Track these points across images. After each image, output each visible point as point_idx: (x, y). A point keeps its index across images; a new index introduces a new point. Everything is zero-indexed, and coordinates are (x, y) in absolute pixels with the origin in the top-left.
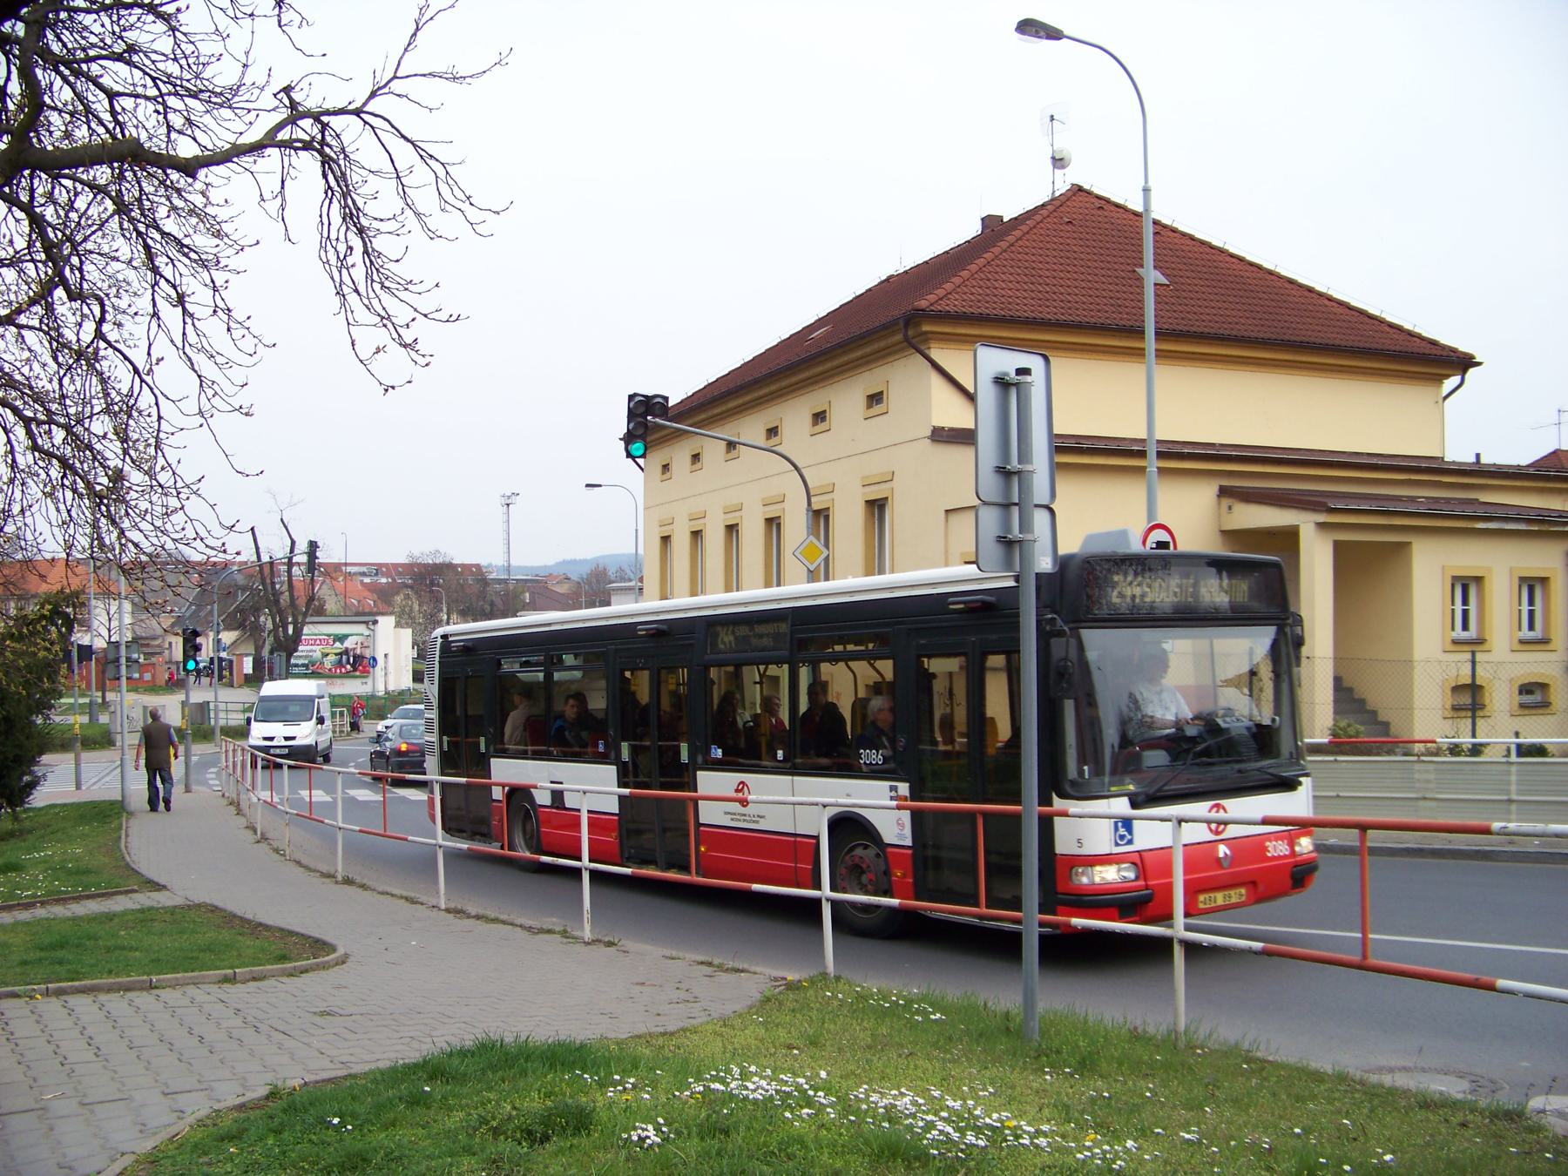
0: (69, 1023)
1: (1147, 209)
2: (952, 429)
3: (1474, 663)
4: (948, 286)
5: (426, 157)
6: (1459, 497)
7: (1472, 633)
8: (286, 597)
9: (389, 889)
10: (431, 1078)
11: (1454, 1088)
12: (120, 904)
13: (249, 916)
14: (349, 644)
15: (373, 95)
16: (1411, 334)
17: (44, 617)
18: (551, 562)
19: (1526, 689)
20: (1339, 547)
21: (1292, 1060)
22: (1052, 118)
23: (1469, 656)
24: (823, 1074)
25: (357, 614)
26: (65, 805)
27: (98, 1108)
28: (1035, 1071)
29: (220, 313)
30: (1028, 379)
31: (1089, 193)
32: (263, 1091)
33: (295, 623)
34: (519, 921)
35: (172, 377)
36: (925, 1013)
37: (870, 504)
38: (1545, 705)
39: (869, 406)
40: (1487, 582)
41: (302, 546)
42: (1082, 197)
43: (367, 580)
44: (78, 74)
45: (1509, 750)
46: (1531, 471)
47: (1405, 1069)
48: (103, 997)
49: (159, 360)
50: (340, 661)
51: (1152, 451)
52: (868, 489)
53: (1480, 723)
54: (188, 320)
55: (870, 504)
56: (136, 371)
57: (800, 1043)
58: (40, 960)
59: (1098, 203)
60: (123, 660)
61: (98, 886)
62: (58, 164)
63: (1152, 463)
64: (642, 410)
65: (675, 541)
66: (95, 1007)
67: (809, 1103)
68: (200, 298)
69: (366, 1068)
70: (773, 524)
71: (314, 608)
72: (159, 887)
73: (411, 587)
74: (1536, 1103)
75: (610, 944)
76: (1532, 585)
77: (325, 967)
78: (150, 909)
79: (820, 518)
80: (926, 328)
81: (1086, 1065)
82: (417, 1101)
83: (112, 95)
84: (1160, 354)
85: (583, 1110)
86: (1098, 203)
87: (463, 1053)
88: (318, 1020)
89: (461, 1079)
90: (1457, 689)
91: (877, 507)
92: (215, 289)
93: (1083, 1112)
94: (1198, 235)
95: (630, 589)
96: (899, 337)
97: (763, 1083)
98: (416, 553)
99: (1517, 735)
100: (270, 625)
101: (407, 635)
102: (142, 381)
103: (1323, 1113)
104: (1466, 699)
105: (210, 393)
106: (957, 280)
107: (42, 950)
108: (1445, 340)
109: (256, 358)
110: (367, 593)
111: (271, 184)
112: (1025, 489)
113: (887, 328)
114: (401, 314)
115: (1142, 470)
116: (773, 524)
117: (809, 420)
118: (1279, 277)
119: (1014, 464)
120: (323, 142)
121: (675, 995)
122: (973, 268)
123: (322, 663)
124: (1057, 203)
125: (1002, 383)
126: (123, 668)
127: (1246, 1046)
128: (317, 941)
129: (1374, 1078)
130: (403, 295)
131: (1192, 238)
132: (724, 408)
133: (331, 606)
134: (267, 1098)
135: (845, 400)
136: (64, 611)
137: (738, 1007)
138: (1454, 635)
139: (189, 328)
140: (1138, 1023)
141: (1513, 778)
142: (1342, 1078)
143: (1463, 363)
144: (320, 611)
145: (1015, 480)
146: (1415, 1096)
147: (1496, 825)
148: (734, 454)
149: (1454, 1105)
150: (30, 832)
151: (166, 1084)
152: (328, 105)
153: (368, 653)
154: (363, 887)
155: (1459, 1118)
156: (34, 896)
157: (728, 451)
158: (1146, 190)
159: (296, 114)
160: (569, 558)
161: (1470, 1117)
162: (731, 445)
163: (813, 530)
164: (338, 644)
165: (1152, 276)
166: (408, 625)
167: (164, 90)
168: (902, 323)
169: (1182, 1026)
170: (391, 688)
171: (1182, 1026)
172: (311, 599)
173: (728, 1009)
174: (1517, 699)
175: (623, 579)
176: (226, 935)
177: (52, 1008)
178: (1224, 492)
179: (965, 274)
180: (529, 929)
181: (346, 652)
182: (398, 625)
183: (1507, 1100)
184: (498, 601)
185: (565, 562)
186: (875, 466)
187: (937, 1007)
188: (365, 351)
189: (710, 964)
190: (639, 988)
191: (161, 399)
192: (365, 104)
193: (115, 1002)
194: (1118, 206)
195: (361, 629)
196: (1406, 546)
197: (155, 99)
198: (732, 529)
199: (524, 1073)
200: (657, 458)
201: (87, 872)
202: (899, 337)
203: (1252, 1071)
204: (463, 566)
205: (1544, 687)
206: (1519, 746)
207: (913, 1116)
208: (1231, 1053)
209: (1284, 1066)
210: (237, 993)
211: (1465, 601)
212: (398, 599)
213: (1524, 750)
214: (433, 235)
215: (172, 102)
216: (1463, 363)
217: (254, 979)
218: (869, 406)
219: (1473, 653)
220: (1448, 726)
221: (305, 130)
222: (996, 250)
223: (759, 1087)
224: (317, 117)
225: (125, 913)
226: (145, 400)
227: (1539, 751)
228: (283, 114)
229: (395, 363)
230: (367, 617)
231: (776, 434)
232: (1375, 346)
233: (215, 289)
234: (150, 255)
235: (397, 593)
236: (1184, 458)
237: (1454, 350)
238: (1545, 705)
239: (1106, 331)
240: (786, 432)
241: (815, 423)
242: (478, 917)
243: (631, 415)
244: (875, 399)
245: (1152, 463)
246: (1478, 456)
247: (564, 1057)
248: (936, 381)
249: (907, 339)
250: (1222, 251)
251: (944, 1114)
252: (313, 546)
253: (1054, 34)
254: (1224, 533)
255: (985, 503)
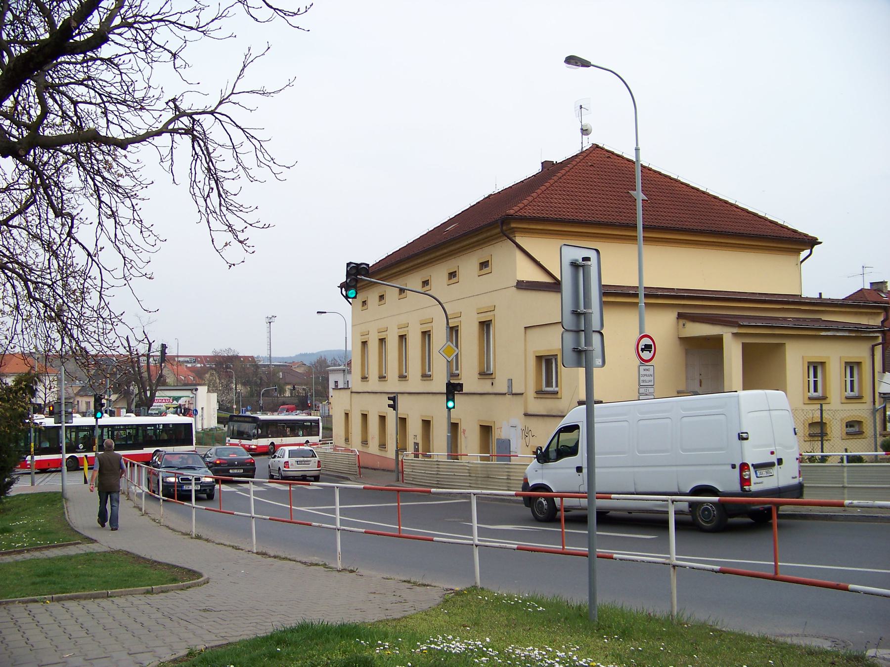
0: (68, 616)
1: (638, 160)
2: (527, 282)
3: (821, 410)
4: (525, 202)
5: (250, 137)
6: (808, 318)
7: (820, 393)
8: (145, 375)
9: (222, 542)
10: (278, 643)
11: (827, 645)
12: (72, 551)
13: (148, 557)
14: (181, 402)
15: (221, 103)
16: (782, 226)
17: (21, 388)
18: (293, 355)
19: (850, 424)
20: (745, 346)
21: (736, 630)
22: (581, 107)
23: (819, 406)
24: (488, 640)
25: (185, 385)
26: (27, 494)
27: (94, 662)
28: (599, 637)
29: (136, 223)
30: (589, 263)
31: (602, 149)
32: (184, 652)
33: (151, 390)
34: (298, 559)
35: (109, 257)
36: (533, 607)
37: (482, 323)
38: (861, 433)
39: (481, 269)
40: (827, 364)
41: (156, 347)
42: (598, 151)
43: (189, 365)
44: (59, 92)
45: (842, 459)
46: (850, 302)
47: (797, 635)
48: (83, 602)
49: (102, 249)
51: (642, 293)
52: (480, 315)
53: (826, 444)
54: (118, 226)
55: (482, 323)
56: (89, 254)
57: (469, 623)
58: (43, 582)
59: (607, 154)
60: (63, 413)
61: (58, 541)
62: (53, 144)
63: (642, 300)
64: (354, 271)
65: (370, 344)
66: (80, 608)
67: (484, 654)
68: (124, 212)
69: (238, 639)
70: (426, 334)
71: (161, 382)
72: (92, 541)
73: (215, 370)
74: (870, 652)
75: (352, 571)
76: (852, 366)
77: (199, 585)
78: (91, 553)
79: (453, 331)
80: (513, 225)
81: (626, 634)
82: (273, 656)
83: (75, 103)
84: (646, 239)
85: (367, 659)
86: (607, 154)
87: (292, 630)
88: (203, 614)
89: (296, 644)
90: (811, 425)
91: (485, 326)
92: (134, 210)
93: (628, 658)
94: (663, 172)
95: (340, 370)
96: (498, 230)
97: (458, 644)
98: (218, 350)
99: (846, 450)
100: (136, 391)
101: (214, 396)
102: (93, 260)
103: (757, 658)
104: (817, 430)
105: (129, 266)
106: (530, 198)
107: (39, 576)
108: (801, 229)
109: (156, 248)
110: (190, 373)
111: (165, 151)
112: (588, 322)
113: (491, 225)
114: (238, 225)
115: (636, 304)
116: (426, 334)
117: (446, 276)
118: (709, 195)
119: (582, 309)
120: (193, 129)
121: (394, 599)
122: (539, 191)
124: (585, 154)
125: (575, 265)
126: (63, 417)
127: (711, 623)
128: (190, 570)
129: (781, 639)
130: (239, 214)
131: (660, 173)
132: (398, 269)
133: (170, 380)
134: (187, 655)
135: (468, 265)
136: (27, 385)
137: (431, 605)
138: (810, 394)
139: (118, 231)
140: (651, 610)
141: (845, 475)
142: (764, 639)
143: (811, 242)
144: (164, 384)
145: (582, 317)
146: (805, 648)
147: (847, 502)
148: (403, 295)
149: (827, 653)
150: (9, 510)
151: (86, 655)
152: (195, 109)
153: (192, 407)
154: (207, 540)
155: (829, 660)
156: (23, 546)
157: (400, 294)
158: (637, 150)
159: (180, 114)
160: (303, 352)
161: (836, 659)
162: (402, 291)
163: (450, 338)
164: (175, 402)
165: (639, 196)
166: (214, 392)
167: (105, 99)
168: (499, 222)
169: (675, 613)
170: (205, 427)
171: (675, 613)
172: (161, 376)
173: (425, 606)
174: (845, 430)
175: (335, 365)
176: (138, 568)
177: (56, 607)
178: (680, 316)
179: (534, 195)
180: (305, 563)
181: (180, 406)
182: (209, 391)
183: (853, 650)
184: (265, 378)
185: (301, 355)
186: (485, 302)
187: (540, 604)
188: (219, 245)
189: (409, 582)
190: (373, 595)
191: (103, 270)
192: (216, 108)
193: (91, 605)
194: (618, 156)
195: (188, 393)
196: (783, 345)
197: (99, 104)
198: (402, 338)
199: (328, 640)
200: (361, 297)
201: (50, 533)
202: (498, 230)
203: (715, 636)
204: (245, 357)
205: (859, 423)
206: (848, 456)
207: (541, 660)
208: (702, 626)
209: (733, 633)
210: (155, 599)
211: (815, 376)
212: (207, 376)
213: (851, 459)
214: (252, 180)
215: (111, 107)
216: (811, 242)
217: (162, 592)
218: (481, 269)
219: (821, 405)
220: (807, 446)
221: (185, 124)
222: (552, 181)
223: (457, 647)
224: (190, 115)
225: (77, 556)
226: (94, 272)
227: (859, 459)
228: (170, 115)
229: (235, 252)
230: (192, 387)
231: (428, 284)
232: (762, 233)
233: (134, 210)
234: (97, 190)
235: (207, 373)
236: (659, 297)
237: (806, 235)
238: (861, 433)
239: (616, 226)
240: (434, 283)
241: (450, 278)
242: (275, 557)
243: (348, 274)
244: (484, 265)
245: (642, 300)
246: (820, 294)
247: (347, 632)
248: (519, 255)
249: (502, 231)
250: (676, 181)
251: (557, 659)
252: (164, 347)
254: (680, 338)
255: (567, 330)
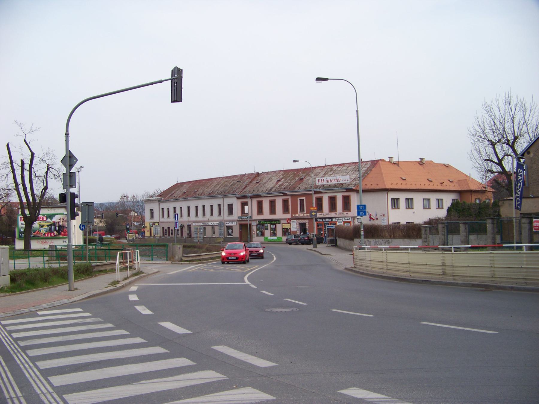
14: (55, 219)
50: (50, 229)
123: (40, 231)
164: (49, 220)
170: (222, 199)
181: (54, 224)
253: (326, 79)
